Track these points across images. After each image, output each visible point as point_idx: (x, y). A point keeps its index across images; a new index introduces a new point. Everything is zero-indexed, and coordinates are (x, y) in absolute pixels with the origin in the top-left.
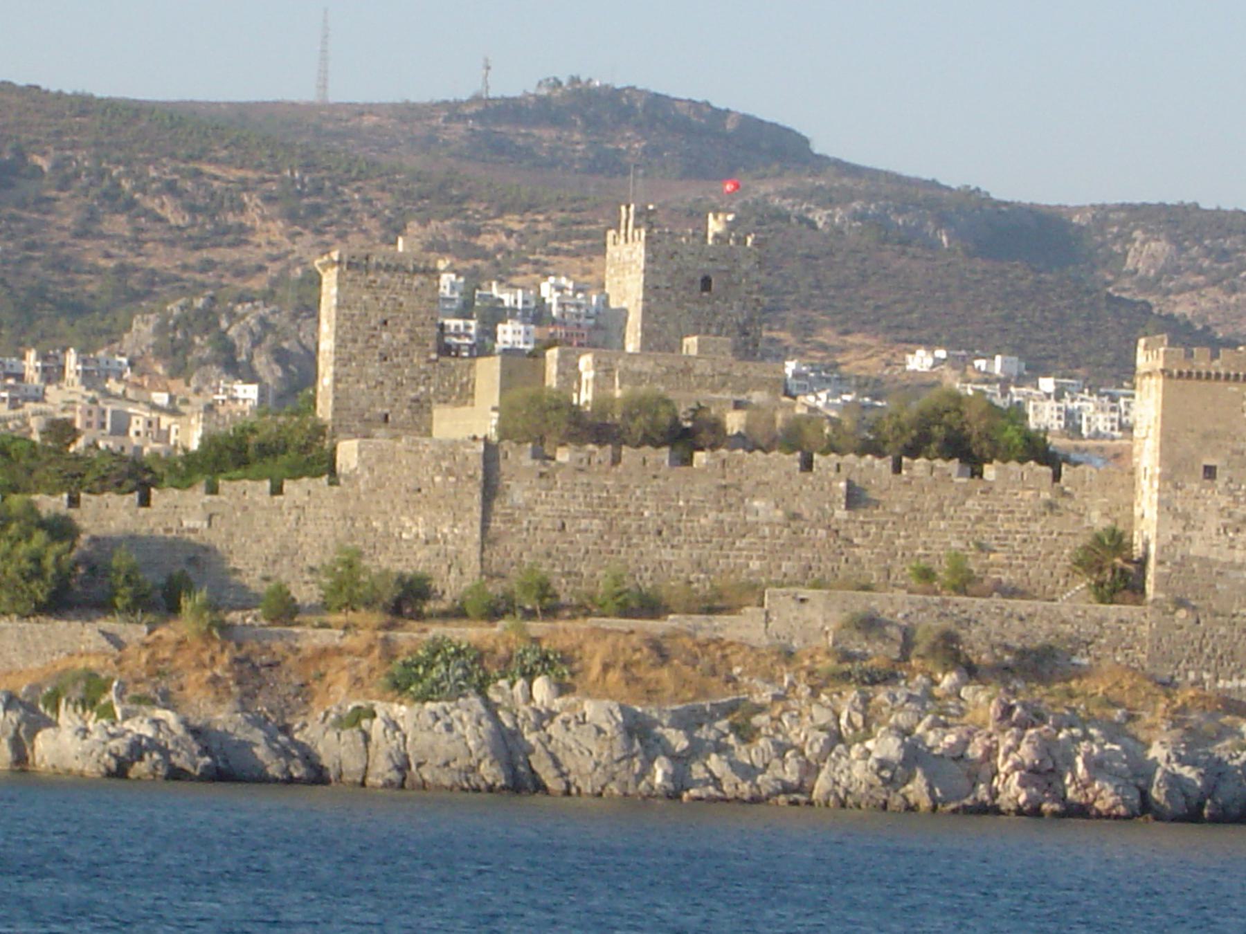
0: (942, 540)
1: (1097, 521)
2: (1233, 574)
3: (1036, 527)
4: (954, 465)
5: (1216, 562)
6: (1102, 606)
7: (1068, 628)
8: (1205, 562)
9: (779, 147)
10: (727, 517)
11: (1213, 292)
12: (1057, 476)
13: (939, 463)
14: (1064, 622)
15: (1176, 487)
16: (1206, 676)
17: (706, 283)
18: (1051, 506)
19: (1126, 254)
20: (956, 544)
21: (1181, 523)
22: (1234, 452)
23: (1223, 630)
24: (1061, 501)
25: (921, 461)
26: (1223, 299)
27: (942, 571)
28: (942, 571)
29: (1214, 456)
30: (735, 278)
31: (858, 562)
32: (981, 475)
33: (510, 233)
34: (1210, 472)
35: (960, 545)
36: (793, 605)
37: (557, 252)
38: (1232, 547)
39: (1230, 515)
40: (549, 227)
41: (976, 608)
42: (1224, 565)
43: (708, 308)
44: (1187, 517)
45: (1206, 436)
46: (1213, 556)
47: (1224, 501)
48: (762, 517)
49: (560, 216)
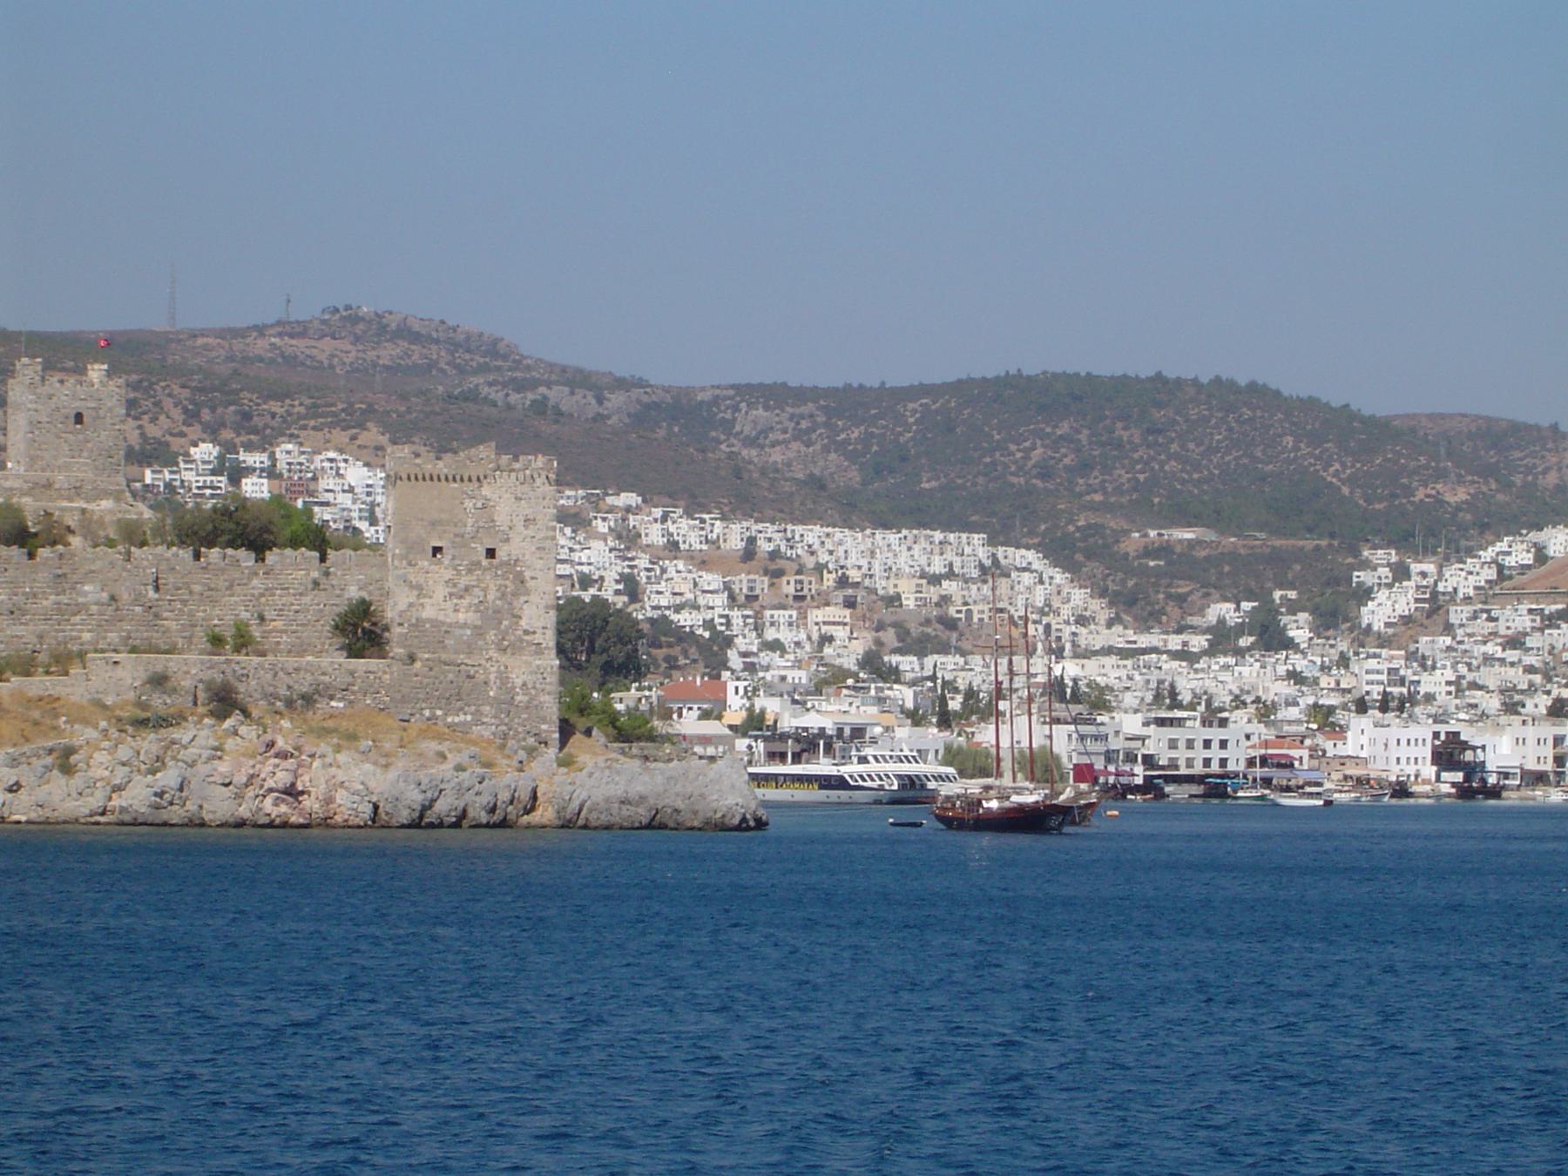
0: (227, 613)
1: (354, 593)
2: (458, 632)
3: (307, 599)
4: (242, 553)
5: (443, 623)
6: (360, 663)
7: (327, 679)
8: (436, 624)
9: (641, 384)
10: (64, 599)
11: (795, 446)
12: (323, 559)
13: (230, 551)
14: (324, 674)
15: (410, 564)
16: (439, 713)
17: (79, 418)
18: (316, 583)
19: (735, 419)
20: (245, 615)
21: (415, 593)
22: (456, 535)
23: (451, 676)
24: (323, 580)
25: (216, 550)
26: (803, 449)
27: (228, 634)
28: (228, 634)
29: (440, 538)
30: (101, 413)
31: (167, 630)
32: (263, 560)
33: (273, 415)
34: (437, 550)
35: (248, 615)
36: (109, 668)
37: (304, 428)
38: (456, 611)
39: (455, 585)
40: (302, 410)
41: (254, 664)
42: (450, 625)
43: (81, 437)
44: (419, 587)
45: (433, 524)
46: (441, 618)
47: (449, 574)
48: (90, 598)
49: (308, 402)
